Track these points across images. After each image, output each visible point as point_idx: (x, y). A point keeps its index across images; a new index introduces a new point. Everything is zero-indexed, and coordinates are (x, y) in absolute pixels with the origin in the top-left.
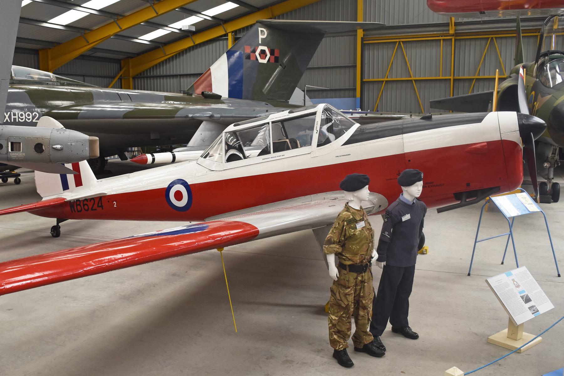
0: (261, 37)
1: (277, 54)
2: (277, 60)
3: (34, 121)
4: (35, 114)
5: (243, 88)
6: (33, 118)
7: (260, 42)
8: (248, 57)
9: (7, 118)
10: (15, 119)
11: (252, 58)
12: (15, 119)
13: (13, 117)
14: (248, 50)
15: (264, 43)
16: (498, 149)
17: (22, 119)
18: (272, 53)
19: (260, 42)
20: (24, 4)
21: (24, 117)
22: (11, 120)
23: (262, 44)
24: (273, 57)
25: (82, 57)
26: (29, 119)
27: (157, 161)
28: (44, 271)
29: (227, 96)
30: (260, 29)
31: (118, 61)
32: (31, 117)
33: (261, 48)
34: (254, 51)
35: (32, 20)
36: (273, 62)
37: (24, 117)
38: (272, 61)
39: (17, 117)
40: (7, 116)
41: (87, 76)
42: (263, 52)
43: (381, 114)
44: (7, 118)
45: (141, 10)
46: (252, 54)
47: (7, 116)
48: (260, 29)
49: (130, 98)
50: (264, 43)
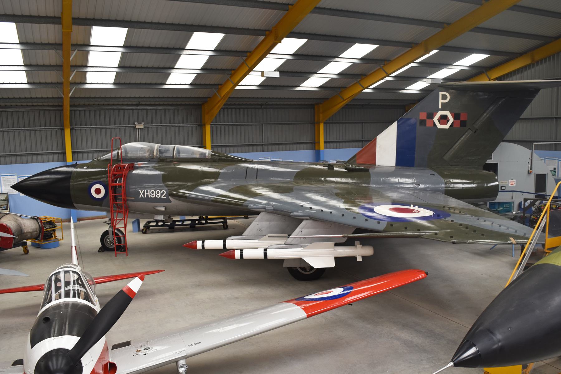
0: (441, 101)
1: (462, 118)
2: (463, 124)
3: (162, 197)
4: (164, 192)
5: (416, 156)
6: (162, 194)
7: (440, 107)
8: (423, 123)
9: (142, 194)
10: (147, 195)
11: (429, 124)
12: (147, 195)
13: (146, 194)
14: (423, 116)
15: (445, 107)
16: (337, 167)
17: (153, 196)
18: (456, 117)
19: (440, 107)
21: (154, 194)
22: (144, 195)
23: (443, 109)
24: (458, 122)
25: (347, 106)
26: (158, 196)
28: (44, 312)
29: (394, 165)
30: (441, 94)
32: (160, 194)
33: (440, 113)
34: (431, 116)
36: (459, 126)
37: (154, 194)
38: (458, 125)
40: (142, 193)
41: (365, 123)
42: (444, 119)
43: (311, 208)
44: (142, 194)
45: (398, 57)
46: (428, 121)
47: (142, 193)
48: (441, 94)
50: (445, 107)
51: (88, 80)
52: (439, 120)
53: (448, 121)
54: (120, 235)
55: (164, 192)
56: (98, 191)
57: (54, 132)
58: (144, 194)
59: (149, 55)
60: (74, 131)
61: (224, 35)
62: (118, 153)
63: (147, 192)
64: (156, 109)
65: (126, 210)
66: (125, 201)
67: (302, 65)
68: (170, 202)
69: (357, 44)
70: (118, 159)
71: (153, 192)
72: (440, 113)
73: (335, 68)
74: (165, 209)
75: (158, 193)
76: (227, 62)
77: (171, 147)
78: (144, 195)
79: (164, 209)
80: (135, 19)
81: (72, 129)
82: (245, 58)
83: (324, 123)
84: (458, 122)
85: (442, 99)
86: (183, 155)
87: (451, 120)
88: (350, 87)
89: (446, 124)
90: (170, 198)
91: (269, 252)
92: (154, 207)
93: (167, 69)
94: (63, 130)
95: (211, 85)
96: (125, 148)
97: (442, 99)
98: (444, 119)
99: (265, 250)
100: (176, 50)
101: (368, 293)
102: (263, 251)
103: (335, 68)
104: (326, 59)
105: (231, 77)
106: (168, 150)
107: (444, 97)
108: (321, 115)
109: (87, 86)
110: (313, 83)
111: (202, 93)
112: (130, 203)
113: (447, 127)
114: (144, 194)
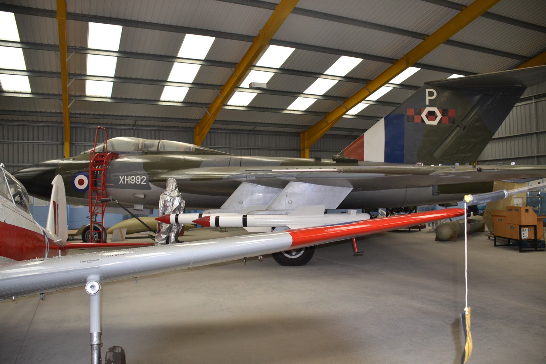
0: (428, 98)
3: (142, 183)
4: (144, 178)
6: (142, 180)
7: (427, 103)
9: (121, 180)
10: (127, 181)
11: (417, 120)
12: (127, 181)
13: (126, 180)
17: (133, 182)
18: (443, 112)
19: (427, 103)
20: (19, 85)
21: (134, 180)
22: (124, 181)
23: (430, 106)
25: (325, 136)
26: (138, 182)
27: (222, 223)
30: (427, 90)
31: (298, 134)
32: (140, 180)
33: (427, 109)
34: (420, 113)
35: (150, 100)
37: (134, 180)
39: (129, 180)
40: (122, 179)
44: (121, 180)
47: (122, 179)
48: (427, 90)
49: (241, 163)
50: (432, 103)
51: (162, 98)
52: (427, 116)
53: (436, 117)
54: (101, 230)
55: (144, 178)
56: (81, 182)
57: (55, 147)
58: (124, 180)
59: (143, 64)
60: (74, 146)
61: (294, 49)
62: (104, 147)
63: (127, 178)
64: (151, 130)
65: (106, 202)
66: (105, 186)
67: (292, 81)
68: (150, 188)
69: (343, 57)
70: (103, 154)
71: (133, 178)
72: (427, 109)
73: (321, 86)
74: (145, 196)
75: (138, 179)
76: (219, 75)
77: (156, 142)
78: (124, 181)
79: (143, 196)
80: (128, 18)
81: (72, 145)
82: (233, 69)
83: (309, 151)
84: (446, 118)
85: (429, 96)
86: (167, 149)
87: (439, 116)
88: (332, 112)
89: (434, 120)
90: (150, 184)
91: (249, 218)
92: (133, 195)
93: (161, 82)
94: (63, 144)
95: (202, 104)
96: (111, 142)
97: (429, 96)
98: (431, 115)
99: (245, 217)
100: (169, 58)
101: (369, 225)
102: (241, 218)
103: (321, 86)
104: (314, 75)
105: (221, 93)
106: (152, 146)
107: (431, 94)
108: (306, 142)
109: (160, 103)
110: (300, 105)
111: (196, 113)
112: (110, 190)
113: (435, 123)
114: (124, 180)
